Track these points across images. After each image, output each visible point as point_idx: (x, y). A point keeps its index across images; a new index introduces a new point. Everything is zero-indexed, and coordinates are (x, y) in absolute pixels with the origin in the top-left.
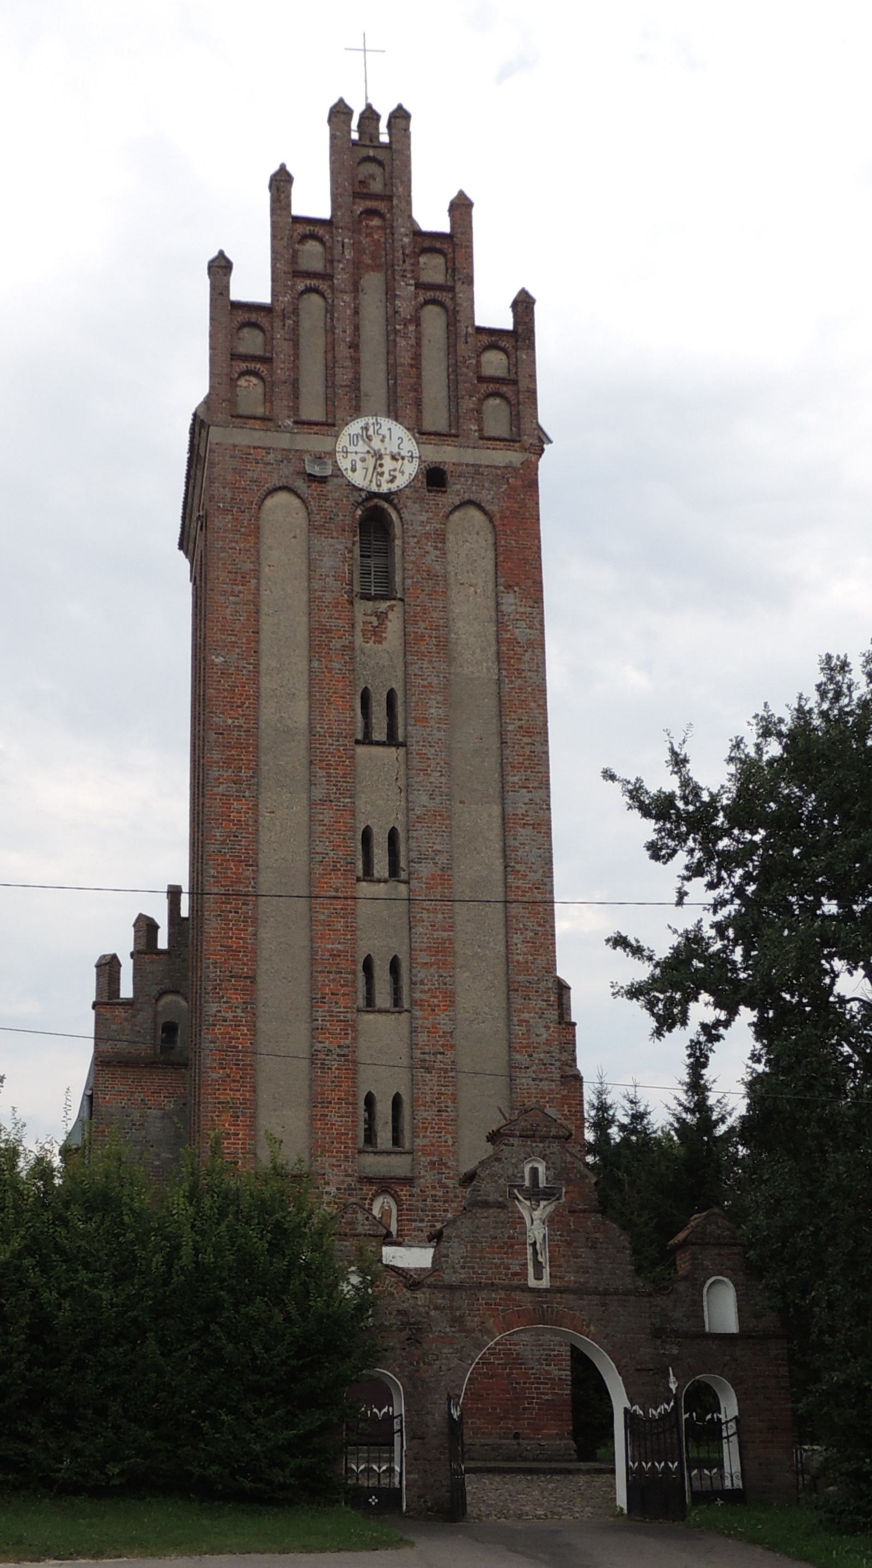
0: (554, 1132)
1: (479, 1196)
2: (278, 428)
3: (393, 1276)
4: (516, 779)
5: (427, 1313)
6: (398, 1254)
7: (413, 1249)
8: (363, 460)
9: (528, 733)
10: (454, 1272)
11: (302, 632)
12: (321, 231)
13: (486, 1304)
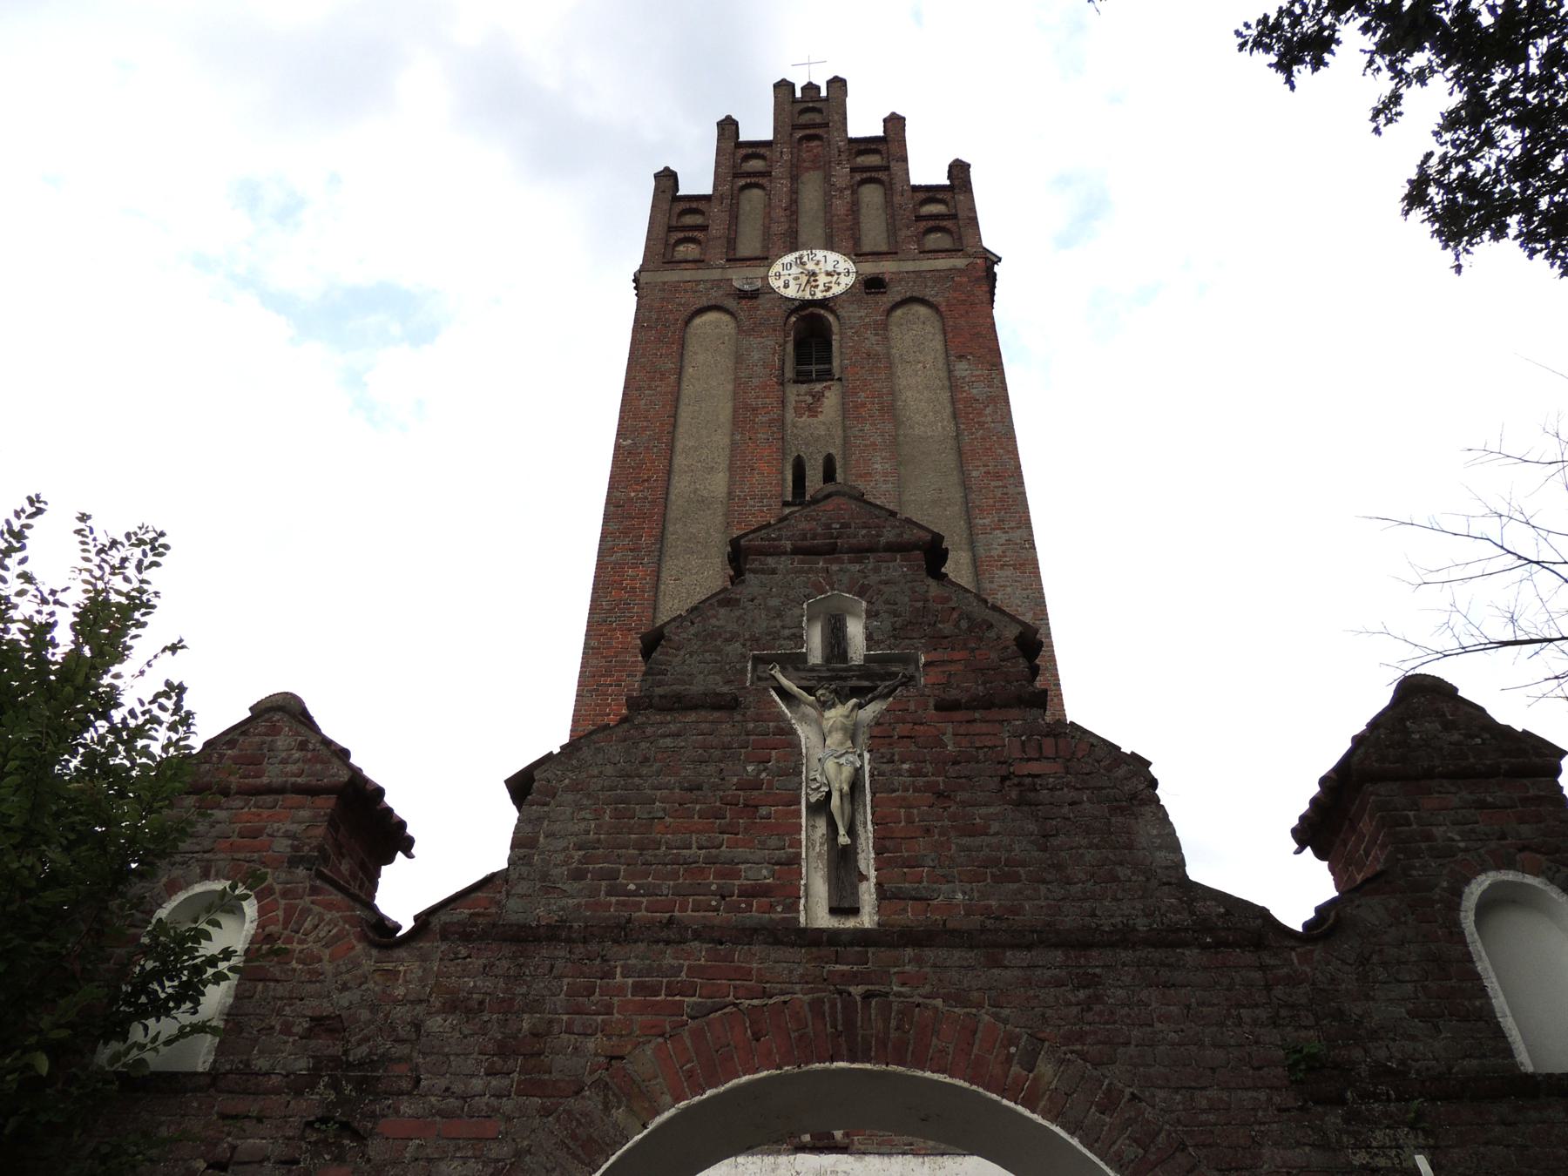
0: (889, 535)
1: (660, 684)
2: (710, 267)
3: (329, 906)
4: (987, 521)
5: (417, 1026)
6: (840, 1168)
7: (868, 1158)
8: (797, 279)
9: (998, 477)
10: (547, 890)
11: (725, 412)
12: (762, 151)
13: (638, 988)
